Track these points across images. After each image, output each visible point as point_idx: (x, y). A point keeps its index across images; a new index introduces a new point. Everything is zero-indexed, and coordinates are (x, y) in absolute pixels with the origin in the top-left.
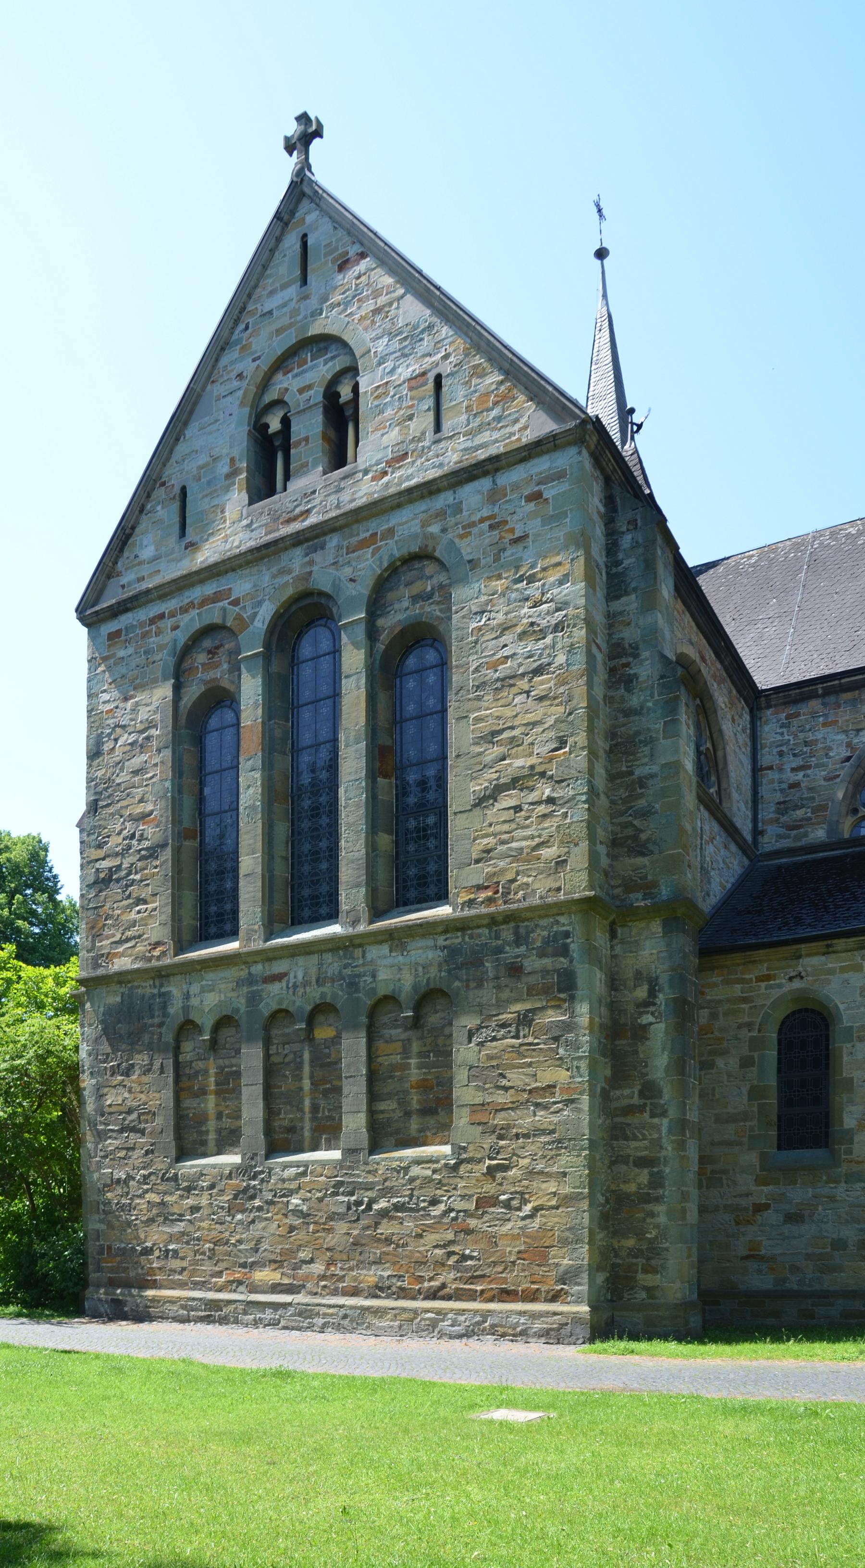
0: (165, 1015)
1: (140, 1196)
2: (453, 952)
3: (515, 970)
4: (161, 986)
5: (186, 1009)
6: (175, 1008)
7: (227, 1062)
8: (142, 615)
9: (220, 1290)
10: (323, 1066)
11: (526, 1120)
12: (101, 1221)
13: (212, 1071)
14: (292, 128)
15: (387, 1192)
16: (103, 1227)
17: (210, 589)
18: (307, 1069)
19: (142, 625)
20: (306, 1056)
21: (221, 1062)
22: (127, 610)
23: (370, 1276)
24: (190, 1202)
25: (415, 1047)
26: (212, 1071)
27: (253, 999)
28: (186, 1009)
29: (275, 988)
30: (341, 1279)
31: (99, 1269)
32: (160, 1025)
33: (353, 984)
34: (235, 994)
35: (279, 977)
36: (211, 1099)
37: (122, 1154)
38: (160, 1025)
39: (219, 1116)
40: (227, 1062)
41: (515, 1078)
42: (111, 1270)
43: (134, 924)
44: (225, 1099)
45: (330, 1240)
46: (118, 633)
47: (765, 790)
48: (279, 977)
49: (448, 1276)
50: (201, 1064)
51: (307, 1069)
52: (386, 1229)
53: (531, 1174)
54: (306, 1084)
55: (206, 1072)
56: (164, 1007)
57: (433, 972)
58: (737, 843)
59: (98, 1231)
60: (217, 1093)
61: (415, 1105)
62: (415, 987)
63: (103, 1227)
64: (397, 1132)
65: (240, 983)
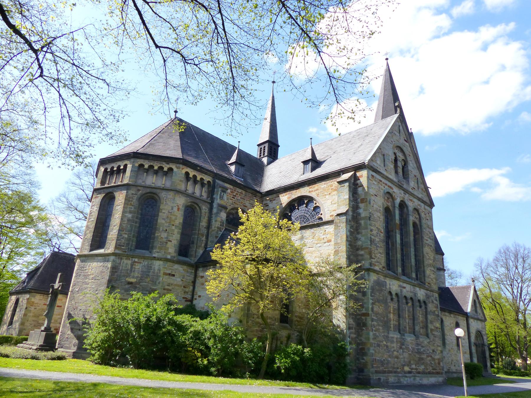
0: (386, 288)
3: (433, 302)
5: (390, 288)
6: (388, 287)
16: (373, 352)
17: (390, 184)
22: (376, 173)
29: (404, 290)
33: (415, 295)
35: (405, 288)
42: (377, 367)
48: (405, 288)
50: (390, 304)
56: (386, 286)
63: (373, 352)
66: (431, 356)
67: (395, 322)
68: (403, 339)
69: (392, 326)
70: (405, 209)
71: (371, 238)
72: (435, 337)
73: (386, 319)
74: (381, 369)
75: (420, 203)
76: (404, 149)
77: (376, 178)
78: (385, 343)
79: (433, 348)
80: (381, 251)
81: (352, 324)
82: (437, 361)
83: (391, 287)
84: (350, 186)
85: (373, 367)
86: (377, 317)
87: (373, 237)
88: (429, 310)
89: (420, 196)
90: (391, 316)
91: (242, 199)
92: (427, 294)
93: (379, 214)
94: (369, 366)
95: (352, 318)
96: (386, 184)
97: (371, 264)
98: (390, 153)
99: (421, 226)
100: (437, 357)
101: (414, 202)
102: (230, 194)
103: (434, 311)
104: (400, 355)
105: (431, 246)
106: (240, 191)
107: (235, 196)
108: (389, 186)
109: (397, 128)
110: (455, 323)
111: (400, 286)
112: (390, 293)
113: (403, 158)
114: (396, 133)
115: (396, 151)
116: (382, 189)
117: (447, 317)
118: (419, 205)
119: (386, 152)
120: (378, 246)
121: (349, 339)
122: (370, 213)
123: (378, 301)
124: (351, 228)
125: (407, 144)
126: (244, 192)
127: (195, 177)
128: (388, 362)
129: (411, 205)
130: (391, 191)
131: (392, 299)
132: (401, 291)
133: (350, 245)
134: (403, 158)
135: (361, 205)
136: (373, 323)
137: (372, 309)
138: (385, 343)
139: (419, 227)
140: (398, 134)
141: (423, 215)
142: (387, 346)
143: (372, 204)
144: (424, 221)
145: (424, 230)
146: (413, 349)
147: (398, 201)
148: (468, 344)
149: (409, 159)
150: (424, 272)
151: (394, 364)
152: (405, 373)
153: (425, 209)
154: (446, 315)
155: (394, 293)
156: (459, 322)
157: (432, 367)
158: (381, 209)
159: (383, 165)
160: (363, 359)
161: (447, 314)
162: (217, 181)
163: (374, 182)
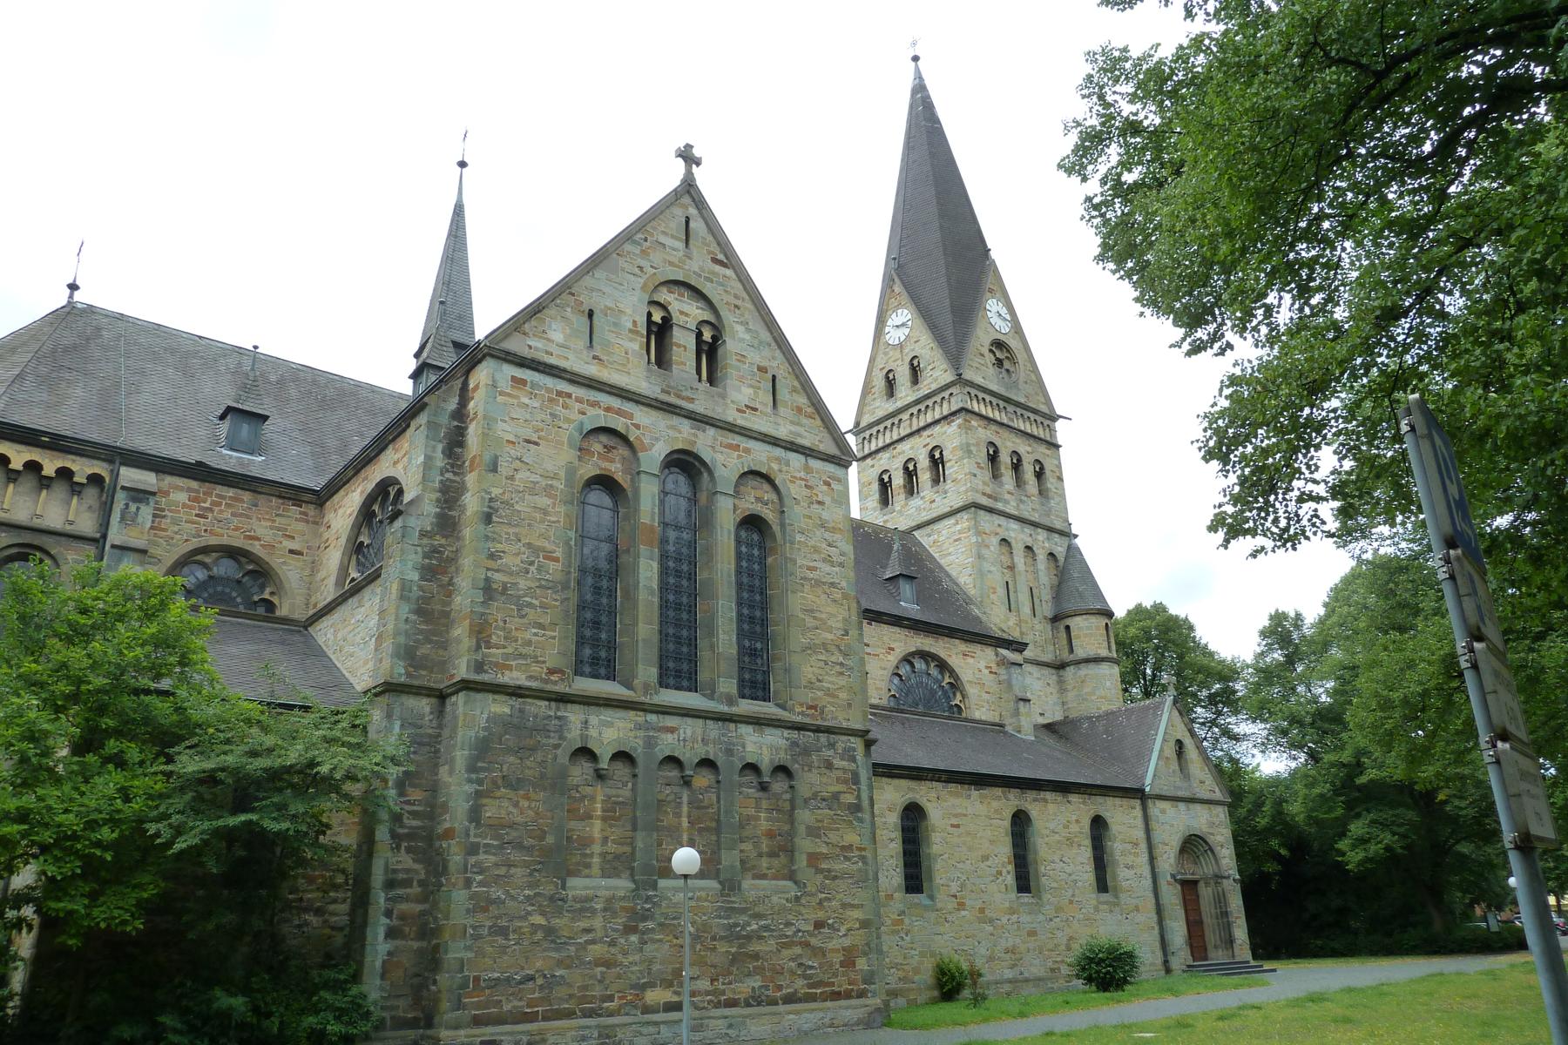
1: (524, 918)
2: (794, 744)
3: (829, 766)
4: (558, 709)
5: (584, 737)
7: (614, 792)
8: (549, 382)
9: (611, 1015)
10: (698, 808)
11: (839, 866)
12: (467, 948)
13: (600, 798)
14: (696, 152)
15: (758, 916)
17: (615, 402)
18: (685, 809)
19: (549, 390)
20: (685, 799)
21: (608, 791)
23: (747, 986)
24: (583, 924)
25: (765, 804)
26: (600, 798)
27: (650, 743)
28: (584, 737)
29: (669, 738)
30: (723, 993)
31: (459, 1006)
32: (556, 747)
33: (729, 752)
34: (632, 734)
35: (672, 730)
36: (598, 824)
37: (502, 871)
38: (556, 747)
39: (605, 840)
40: (614, 792)
41: (833, 837)
42: (478, 1006)
43: (529, 643)
44: (611, 826)
45: (712, 958)
46: (523, 382)
47: (1159, 835)
48: (672, 730)
49: (800, 985)
50: (589, 790)
51: (685, 809)
52: (755, 947)
53: (844, 906)
54: (685, 824)
55: (593, 799)
56: (560, 731)
57: (782, 755)
58: (652, 712)
59: (462, 960)
60: (604, 819)
61: (765, 849)
62: (771, 761)
64: (754, 867)
65: (638, 727)
66: (807, 944)
67: (611, 847)
68: (648, 899)
69: (596, 860)
70: (705, 475)
71: (487, 580)
72: (835, 878)
73: (550, 839)
74: (507, 1007)
75: (779, 452)
76: (707, 289)
77: (533, 385)
78: (538, 920)
79: (821, 915)
80: (546, 620)
81: (407, 871)
82: (837, 959)
83: (593, 732)
84: (432, 426)
85: (459, 1006)
86: (497, 837)
87: (497, 576)
88: (804, 790)
89: (783, 432)
90: (596, 828)
91: (241, 515)
92: (794, 744)
93: (544, 501)
94: (445, 1005)
95: (408, 850)
96: (594, 404)
97: (479, 667)
98: (628, 306)
99: (783, 525)
100: (836, 943)
101: (747, 451)
102: (184, 505)
103: (836, 796)
104: (625, 954)
105: (833, 585)
106: (231, 492)
107: (211, 510)
108: (608, 409)
109: (676, 224)
110: (1086, 823)
111: (648, 727)
112: (585, 753)
113: (708, 316)
114: (668, 241)
115: (664, 296)
116: (567, 420)
117: (1051, 807)
118: (778, 460)
119: (598, 303)
120: (530, 605)
121: (384, 920)
122: (491, 500)
123: (513, 784)
124: (426, 556)
125: (729, 272)
126: (247, 496)
127: (33, 467)
128: (551, 982)
129: (725, 460)
130: (619, 424)
131: (600, 776)
132: (650, 743)
133: (419, 612)
134: (708, 316)
135: (471, 479)
136: (472, 860)
137: (475, 815)
138: (538, 920)
139: (776, 528)
140: (681, 245)
141: (795, 490)
142: (550, 931)
143: (504, 468)
144: (798, 514)
145: (799, 537)
146: (705, 927)
147: (653, 455)
148: (1148, 882)
149: (728, 317)
150: (787, 671)
151: (585, 988)
152: (647, 1010)
153: (807, 469)
154: (1045, 801)
155: (605, 754)
156: (1106, 815)
157: (805, 977)
158: (560, 485)
159: (581, 343)
160: (435, 982)
161: (1049, 795)
162: (124, 471)
163: (526, 401)
